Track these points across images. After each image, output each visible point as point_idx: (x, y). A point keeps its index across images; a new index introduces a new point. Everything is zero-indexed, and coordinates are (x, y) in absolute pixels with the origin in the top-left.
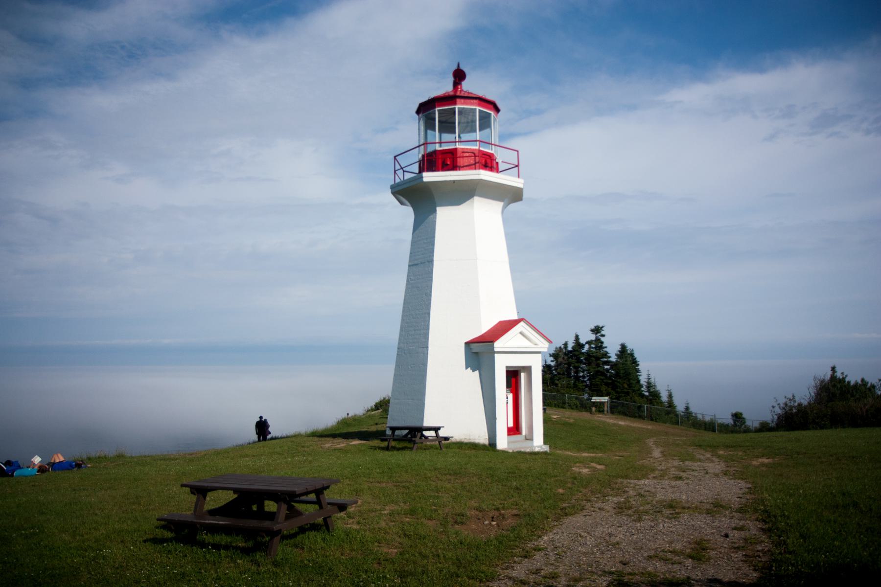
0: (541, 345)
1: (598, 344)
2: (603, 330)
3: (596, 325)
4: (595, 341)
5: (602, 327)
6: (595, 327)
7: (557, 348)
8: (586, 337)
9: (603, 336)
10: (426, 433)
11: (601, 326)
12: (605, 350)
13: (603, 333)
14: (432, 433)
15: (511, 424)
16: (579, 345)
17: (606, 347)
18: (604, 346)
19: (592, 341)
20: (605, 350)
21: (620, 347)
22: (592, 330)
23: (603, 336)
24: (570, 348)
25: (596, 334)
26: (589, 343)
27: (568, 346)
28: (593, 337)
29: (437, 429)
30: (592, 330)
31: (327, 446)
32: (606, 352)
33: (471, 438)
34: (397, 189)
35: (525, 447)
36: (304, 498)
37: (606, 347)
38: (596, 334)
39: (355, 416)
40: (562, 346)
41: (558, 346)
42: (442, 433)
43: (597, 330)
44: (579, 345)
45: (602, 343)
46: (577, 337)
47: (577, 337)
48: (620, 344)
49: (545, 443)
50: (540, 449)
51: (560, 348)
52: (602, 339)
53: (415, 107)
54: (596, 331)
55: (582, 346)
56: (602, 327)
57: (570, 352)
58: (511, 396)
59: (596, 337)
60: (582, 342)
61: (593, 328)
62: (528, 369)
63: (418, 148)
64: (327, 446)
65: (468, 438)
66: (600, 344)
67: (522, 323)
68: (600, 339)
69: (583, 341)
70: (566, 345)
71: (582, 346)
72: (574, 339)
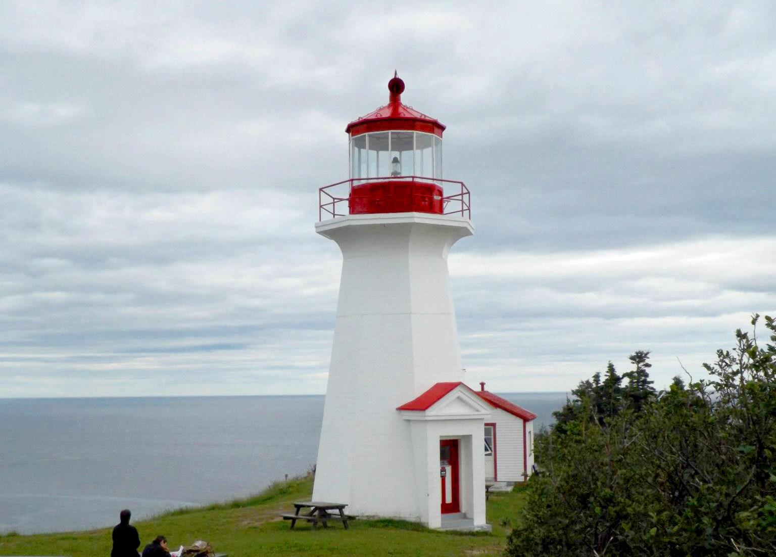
0: (483, 411)
1: (640, 377)
2: (648, 358)
3: (638, 351)
4: (637, 372)
5: (648, 353)
6: (637, 353)
7: (583, 382)
8: (624, 367)
9: (648, 365)
10: (329, 511)
11: (645, 352)
12: (651, 385)
13: (647, 361)
14: (337, 511)
15: (449, 500)
16: (614, 379)
17: (652, 382)
18: (648, 379)
19: (632, 372)
20: (651, 385)
21: (673, 382)
22: (632, 358)
23: (648, 365)
24: (601, 383)
25: (638, 363)
26: (629, 375)
27: (601, 378)
28: (633, 368)
29: (341, 508)
30: (632, 358)
31: (63, 111)
32: (652, 388)
33: (401, 516)
34: (322, 229)
35: (464, 527)
36: (338, 200)
37: (652, 382)
38: (638, 363)
39: (297, 479)
40: (591, 381)
41: (585, 380)
42: (347, 512)
43: (639, 357)
44: (614, 379)
45: (647, 375)
46: (611, 369)
47: (611, 369)
48: (673, 377)
49: (487, 523)
50: (479, 529)
51: (588, 382)
52: (648, 370)
53: (345, 127)
54: (637, 360)
55: (618, 380)
56: (648, 353)
57: (602, 388)
58: (449, 469)
59: (638, 368)
60: (618, 375)
61: (634, 354)
62: (468, 438)
63: (333, 213)
64: (63, 111)
65: (398, 515)
66: (643, 378)
67: (458, 388)
68: (644, 371)
69: (619, 373)
70: (597, 377)
71: (618, 380)
72: (607, 369)
